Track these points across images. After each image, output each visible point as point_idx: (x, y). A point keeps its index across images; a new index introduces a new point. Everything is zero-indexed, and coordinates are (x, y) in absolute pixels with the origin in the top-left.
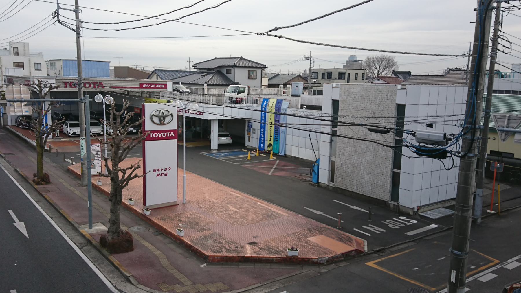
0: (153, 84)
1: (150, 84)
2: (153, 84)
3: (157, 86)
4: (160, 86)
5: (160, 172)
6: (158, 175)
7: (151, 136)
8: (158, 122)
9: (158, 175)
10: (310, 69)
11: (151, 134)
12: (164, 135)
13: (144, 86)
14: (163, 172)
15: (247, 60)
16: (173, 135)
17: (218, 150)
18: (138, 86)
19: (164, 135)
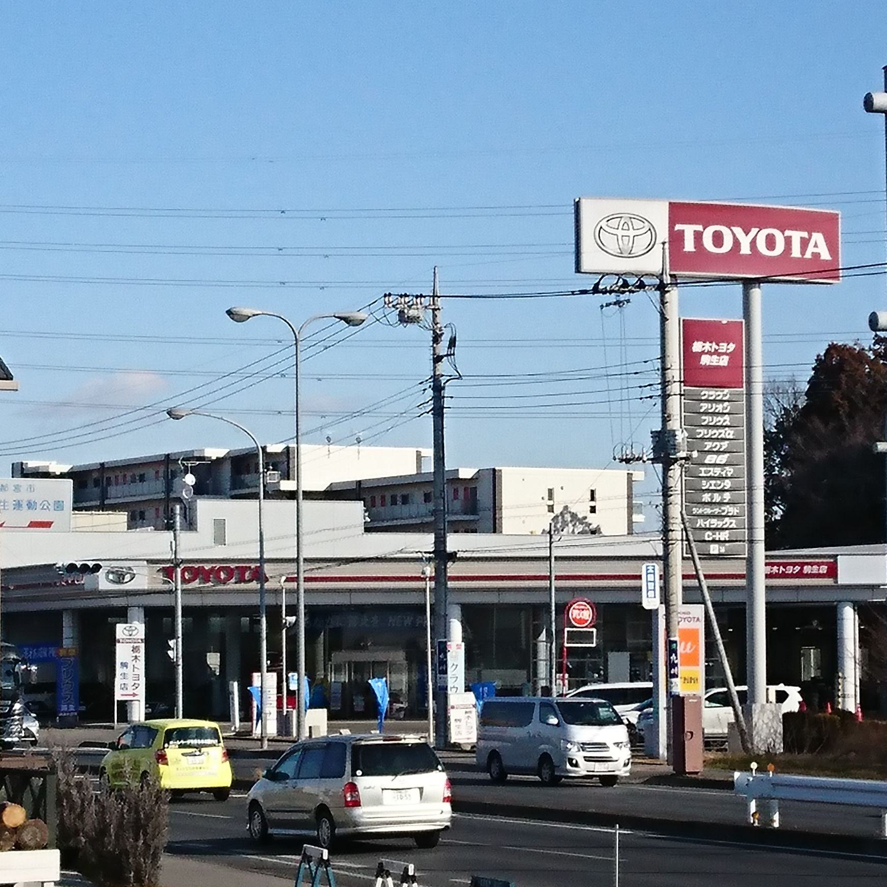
0: (794, 565)
1: (785, 565)
2: (794, 565)
10: (654, 460)
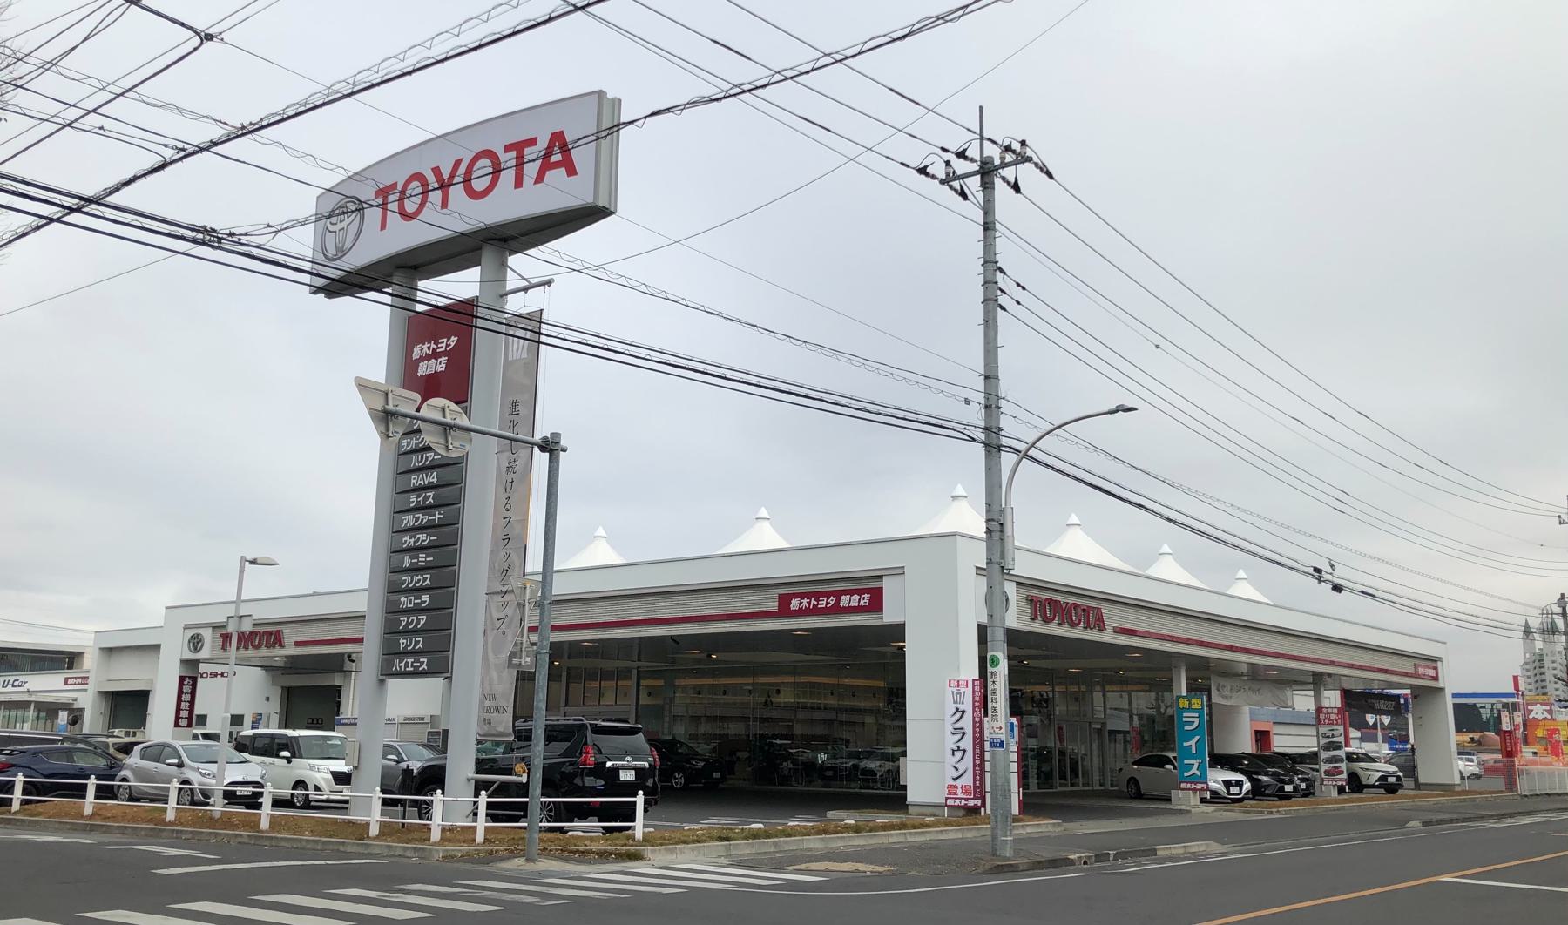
0: (828, 594)
2: (828, 594)
3: (845, 601)
4: (854, 601)
13: (795, 604)
15: (503, 116)
18: (776, 609)
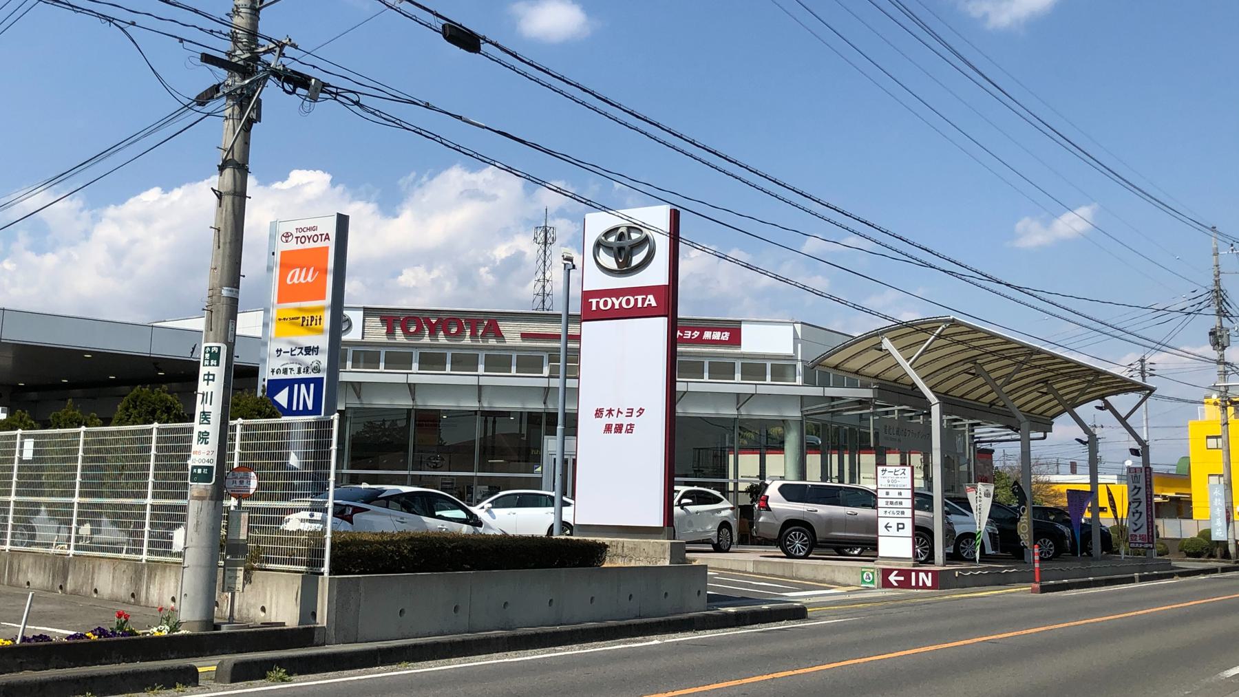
3: (707, 335)
5: (614, 421)
6: (608, 428)
7: (594, 308)
8: (615, 266)
9: (608, 428)
11: (594, 301)
12: (628, 302)
14: (624, 420)
16: (654, 304)
17: (740, 322)
19: (628, 302)
